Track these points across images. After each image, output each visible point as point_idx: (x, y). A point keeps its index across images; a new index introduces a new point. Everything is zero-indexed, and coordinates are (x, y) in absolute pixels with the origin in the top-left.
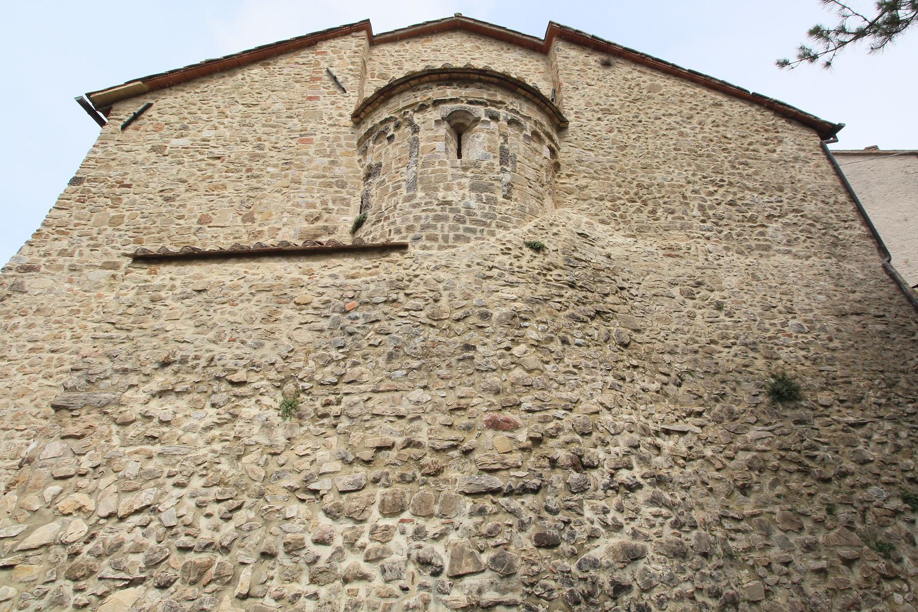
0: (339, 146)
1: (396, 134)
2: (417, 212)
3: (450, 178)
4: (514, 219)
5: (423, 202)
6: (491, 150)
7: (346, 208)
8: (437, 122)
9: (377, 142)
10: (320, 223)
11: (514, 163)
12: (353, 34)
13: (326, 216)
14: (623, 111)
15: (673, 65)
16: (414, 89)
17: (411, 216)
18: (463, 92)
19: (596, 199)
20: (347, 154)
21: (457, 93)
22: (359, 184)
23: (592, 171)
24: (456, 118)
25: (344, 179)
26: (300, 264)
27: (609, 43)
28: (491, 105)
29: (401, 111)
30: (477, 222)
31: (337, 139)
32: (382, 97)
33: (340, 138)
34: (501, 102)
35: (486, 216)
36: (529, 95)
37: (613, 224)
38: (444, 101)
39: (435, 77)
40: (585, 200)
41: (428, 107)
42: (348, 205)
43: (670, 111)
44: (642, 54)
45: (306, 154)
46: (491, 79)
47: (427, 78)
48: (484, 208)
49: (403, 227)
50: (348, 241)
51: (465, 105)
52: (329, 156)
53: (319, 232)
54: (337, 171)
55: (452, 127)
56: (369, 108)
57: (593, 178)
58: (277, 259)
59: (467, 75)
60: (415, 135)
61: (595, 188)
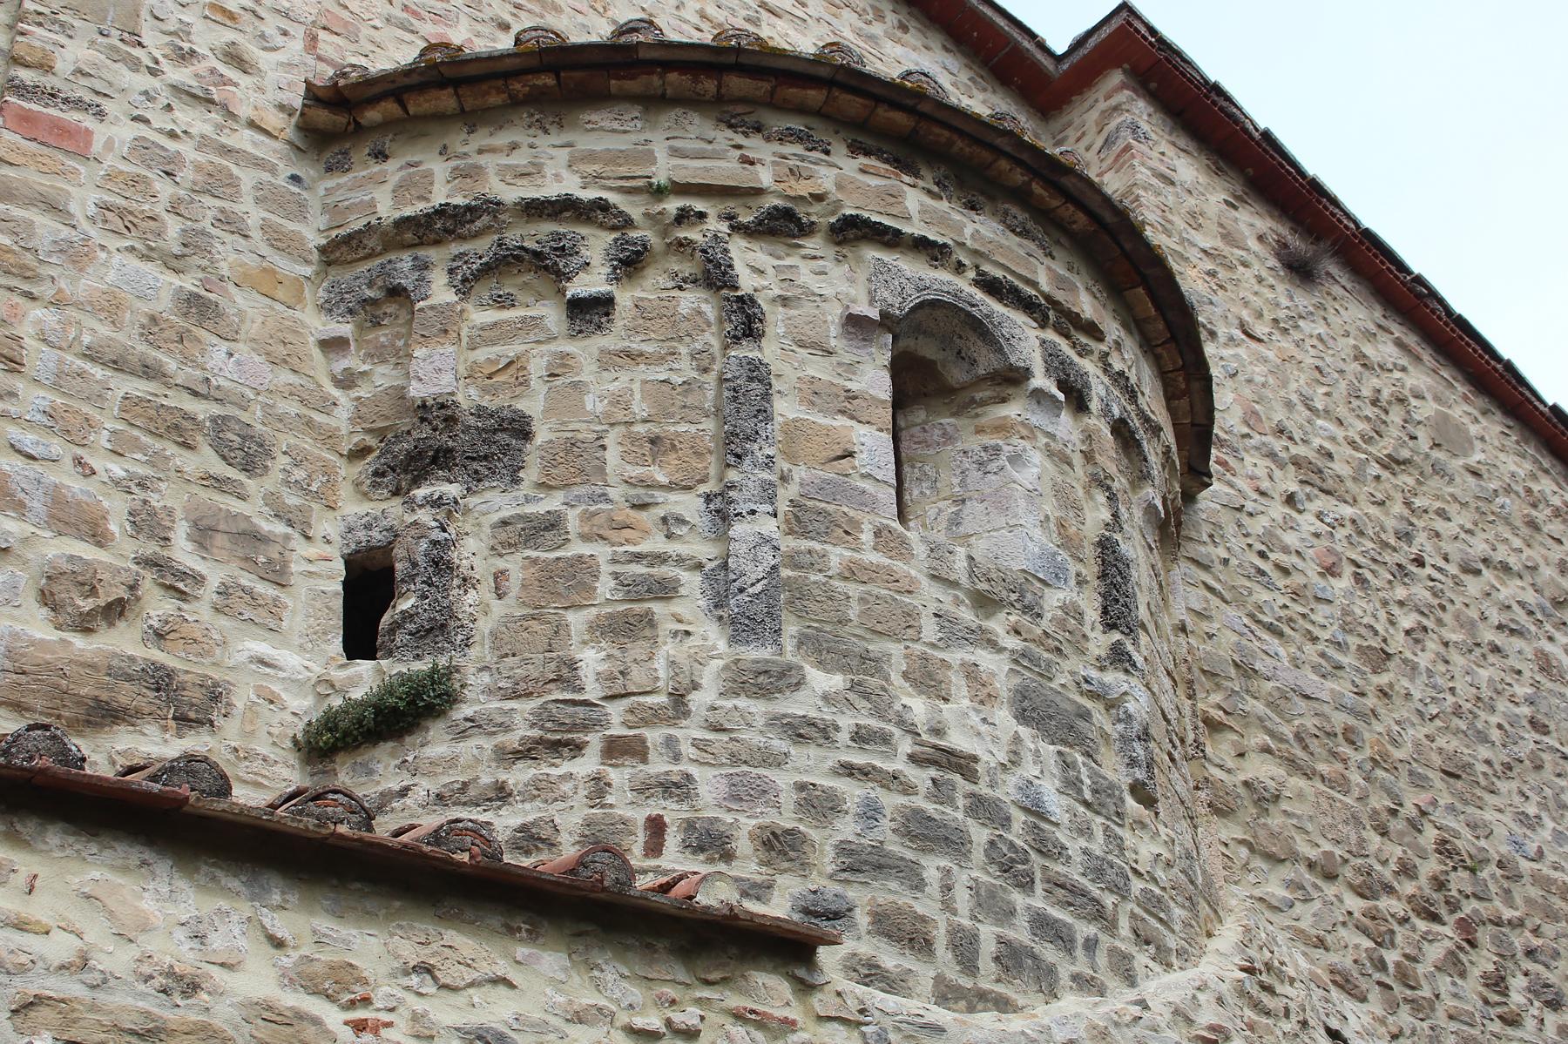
0: (227, 221)
1: (625, 298)
2: (814, 764)
3: (930, 629)
5: (847, 722)
6: (1069, 543)
7: (264, 589)
8: (855, 324)
9: (483, 291)
10: (123, 642)
13: (157, 606)
14: (1362, 492)
15: (1509, 366)
16: (735, 113)
17: (783, 780)
18: (977, 230)
19: (1311, 865)
20: (266, 283)
21: (943, 220)
22: (328, 471)
23: (1287, 731)
25: (253, 416)
26: (280, 924)
27: (1316, 187)
29: (659, 192)
31: (217, 184)
32: (548, 80)
33: (233, 183)
35: (1097, 870)
38: (889, 238)
39: (852, 105)
40: (1274, 859)
41: (806, 230)
42: (277, 575)
43: (1502, 554)
44: (1419, 280)
45: (54, 207)
47: (814, 96)
49: (744, 826)
50: (263, 779)
51: (964, 285)
52: (173, 262)
53: (126, 695)
54: (221, 362)
56: (446, 100)
58: (134, 854)
59: (986, 155)
60: (746, 351)
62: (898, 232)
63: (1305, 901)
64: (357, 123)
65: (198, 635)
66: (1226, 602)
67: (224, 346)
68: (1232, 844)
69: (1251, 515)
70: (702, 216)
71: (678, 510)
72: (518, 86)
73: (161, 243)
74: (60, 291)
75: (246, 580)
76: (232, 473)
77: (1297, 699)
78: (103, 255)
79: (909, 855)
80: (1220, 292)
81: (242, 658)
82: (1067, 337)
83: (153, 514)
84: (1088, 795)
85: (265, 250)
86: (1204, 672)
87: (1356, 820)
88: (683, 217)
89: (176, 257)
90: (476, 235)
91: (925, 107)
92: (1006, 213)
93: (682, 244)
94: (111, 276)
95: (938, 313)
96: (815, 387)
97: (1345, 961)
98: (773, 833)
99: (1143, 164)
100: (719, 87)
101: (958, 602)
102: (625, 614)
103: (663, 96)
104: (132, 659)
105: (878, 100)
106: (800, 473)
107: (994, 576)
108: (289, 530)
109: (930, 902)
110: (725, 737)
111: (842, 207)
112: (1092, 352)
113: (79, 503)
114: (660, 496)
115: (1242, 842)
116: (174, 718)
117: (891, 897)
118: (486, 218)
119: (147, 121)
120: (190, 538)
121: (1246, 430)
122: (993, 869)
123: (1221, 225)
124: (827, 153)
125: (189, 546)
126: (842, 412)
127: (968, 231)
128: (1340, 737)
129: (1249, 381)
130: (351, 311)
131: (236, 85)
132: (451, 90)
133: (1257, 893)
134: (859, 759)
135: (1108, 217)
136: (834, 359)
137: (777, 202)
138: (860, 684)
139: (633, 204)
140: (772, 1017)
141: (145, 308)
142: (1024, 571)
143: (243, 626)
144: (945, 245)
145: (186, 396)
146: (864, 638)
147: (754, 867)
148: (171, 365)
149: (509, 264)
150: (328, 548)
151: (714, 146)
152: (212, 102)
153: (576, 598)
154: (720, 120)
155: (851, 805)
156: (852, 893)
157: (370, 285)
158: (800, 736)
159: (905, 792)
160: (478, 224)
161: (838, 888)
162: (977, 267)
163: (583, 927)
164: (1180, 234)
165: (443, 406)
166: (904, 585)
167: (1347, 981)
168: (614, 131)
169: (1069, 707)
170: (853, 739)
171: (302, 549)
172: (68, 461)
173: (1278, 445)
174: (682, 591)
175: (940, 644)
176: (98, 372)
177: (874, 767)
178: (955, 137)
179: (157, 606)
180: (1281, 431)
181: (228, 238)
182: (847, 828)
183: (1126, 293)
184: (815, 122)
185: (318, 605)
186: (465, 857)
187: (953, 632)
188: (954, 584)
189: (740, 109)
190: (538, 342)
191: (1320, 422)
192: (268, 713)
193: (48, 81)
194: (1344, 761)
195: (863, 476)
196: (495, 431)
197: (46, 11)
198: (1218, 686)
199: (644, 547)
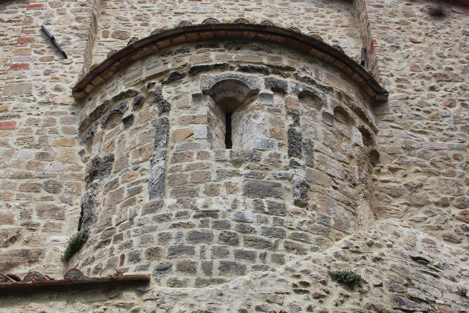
1: (136, 114)
2: (164, 227)
3: (214, 176)
5: (174, 213)
8: (196, 97)
9: (109, 125)
11: (310, 153)
16: (163, 52)
17: (155, 234)
19: (437, 204)
20: (63, 143)
21: (225, 57)
22: (78, 186)
23: (427, 163)
24: (223, 90)
28: (274, 73)
29: (143, 82)
30: (255, 242)
32: (118, 64)
35: (268, 232)
36: (328, 57)
38: (206, 69)
39: (193, 36)
40: (419, 206)
41: (183, 76)
42: (61, 217)
46: (274, 37)
47: (182, 38)
48: (266, 221)
53: (15, 260)
54: (48, 167)
55: (217, 103)
56: (99, 79)
60: (164, 116)
62: (207, 66)
63: (433, 216)
64: (87, 93)
65: (37, 239)
66: (402, 129)
67: (49, 163)
68: (400, 206)
69: (413, 99)
70: (154, 84)
71: (143, 167)
72: (112, 68)
73: (33, 143)
74: (5, 164)
75: (52, 221)
76: (50, 195)
77: (431, 151)
78: (17, 151)
79: (191, 245)
80: (403, 33)
81: (49, 241)
82: (279, 74)
83: (26, 212)
84: (266, 210)
85: (63, 135)
86: (389, 154)
87: (458, 184)
88: (149, 86)
89: (38, 145)
90: (106, 111)
91: (213, 28)
92: (252, 46)
93: (150, 93)
94: (19, 156)
95: (226, 83)
96: (183, 119)
97: (451, 232)
98: (151, 250)
99: (369, 5)
100: (157, 46)
101: (226, 166)
102: (129, 200)
103: (147, 55)
104: (17, 250)
105: (199, 31)
106: (177, 145)
107: (240, 154)
108: (66, 204)
109: (196, 257)
110: (142, 227)
111: (191, 65)
112: (290, 75)
113: (5, 215)
114: (140, 165)
115: (404, 204)
116: (28, 262)
117: (184, 259)
118: (106, 106)
119: (31, 114)
120: (37, 215)
121: (412, 72)
122: (221, 242)
123: (404, 12)
124: (189, 52)
125: (37, 217)
126: (191, 123)
127: (233, 57)
128: (452, 159)
129: (414, 57)
130: (85, 142)
131: (57, 96)
132: (99, 76)
133: (411, 218)
134: (177, 222)
135: (289, 34)
136: (190, 109)
137: (172, 72)
138: (180, 200)
139: (138, 88)
140: (127, 303)
141: (27, 161)
142: (254, 149)
143: (51, 233)
144: (224, 64)
145: (38, 179)
146: (192, 186)
147: (146, 261)
148: (33, 172)
149: (113, 116)
150: (77, 206)
151: (158, 63)
152: (51, 102)
153: (119, 200)
154: (160, 55)
155: (174, 236)
156: (172, 261)
157: (88, 134)
158: (161, 220)
159: (191, 227)
160: (105, 108)
161: (168, 261)
162: (239, 66)
163: (74, 292)
164: (385, 21)
165: (96, 160)
166: (206, 166)
167: (450, 238)
168: (135, 70)
169: (269, 185)
170: (176, 216)
171: (69, 208)
172: (4, 206)
173: (426, 73)
174: (143, 189)
175: (218, 180)
176: (14, 181)
177: (181, 223)
178: (227, 32)
179: (26, 234)
180: (428, 68)
181: (52, 135)
182: (172, 243)
183: (311, 52)
184: (183, 45)
185: (72, 222)
186: (31, 282)
187: (221, 174)
188: (225, 161)
189: (165, 50)
190: (118, 134)
191: (446, 60)
192: (55, 254)
193: (8, 113)
194: (453, 166)
195: (196, 139)
196: (107, 162)
197: (7, 96)
198: (396, 157)
199: (137, 180)
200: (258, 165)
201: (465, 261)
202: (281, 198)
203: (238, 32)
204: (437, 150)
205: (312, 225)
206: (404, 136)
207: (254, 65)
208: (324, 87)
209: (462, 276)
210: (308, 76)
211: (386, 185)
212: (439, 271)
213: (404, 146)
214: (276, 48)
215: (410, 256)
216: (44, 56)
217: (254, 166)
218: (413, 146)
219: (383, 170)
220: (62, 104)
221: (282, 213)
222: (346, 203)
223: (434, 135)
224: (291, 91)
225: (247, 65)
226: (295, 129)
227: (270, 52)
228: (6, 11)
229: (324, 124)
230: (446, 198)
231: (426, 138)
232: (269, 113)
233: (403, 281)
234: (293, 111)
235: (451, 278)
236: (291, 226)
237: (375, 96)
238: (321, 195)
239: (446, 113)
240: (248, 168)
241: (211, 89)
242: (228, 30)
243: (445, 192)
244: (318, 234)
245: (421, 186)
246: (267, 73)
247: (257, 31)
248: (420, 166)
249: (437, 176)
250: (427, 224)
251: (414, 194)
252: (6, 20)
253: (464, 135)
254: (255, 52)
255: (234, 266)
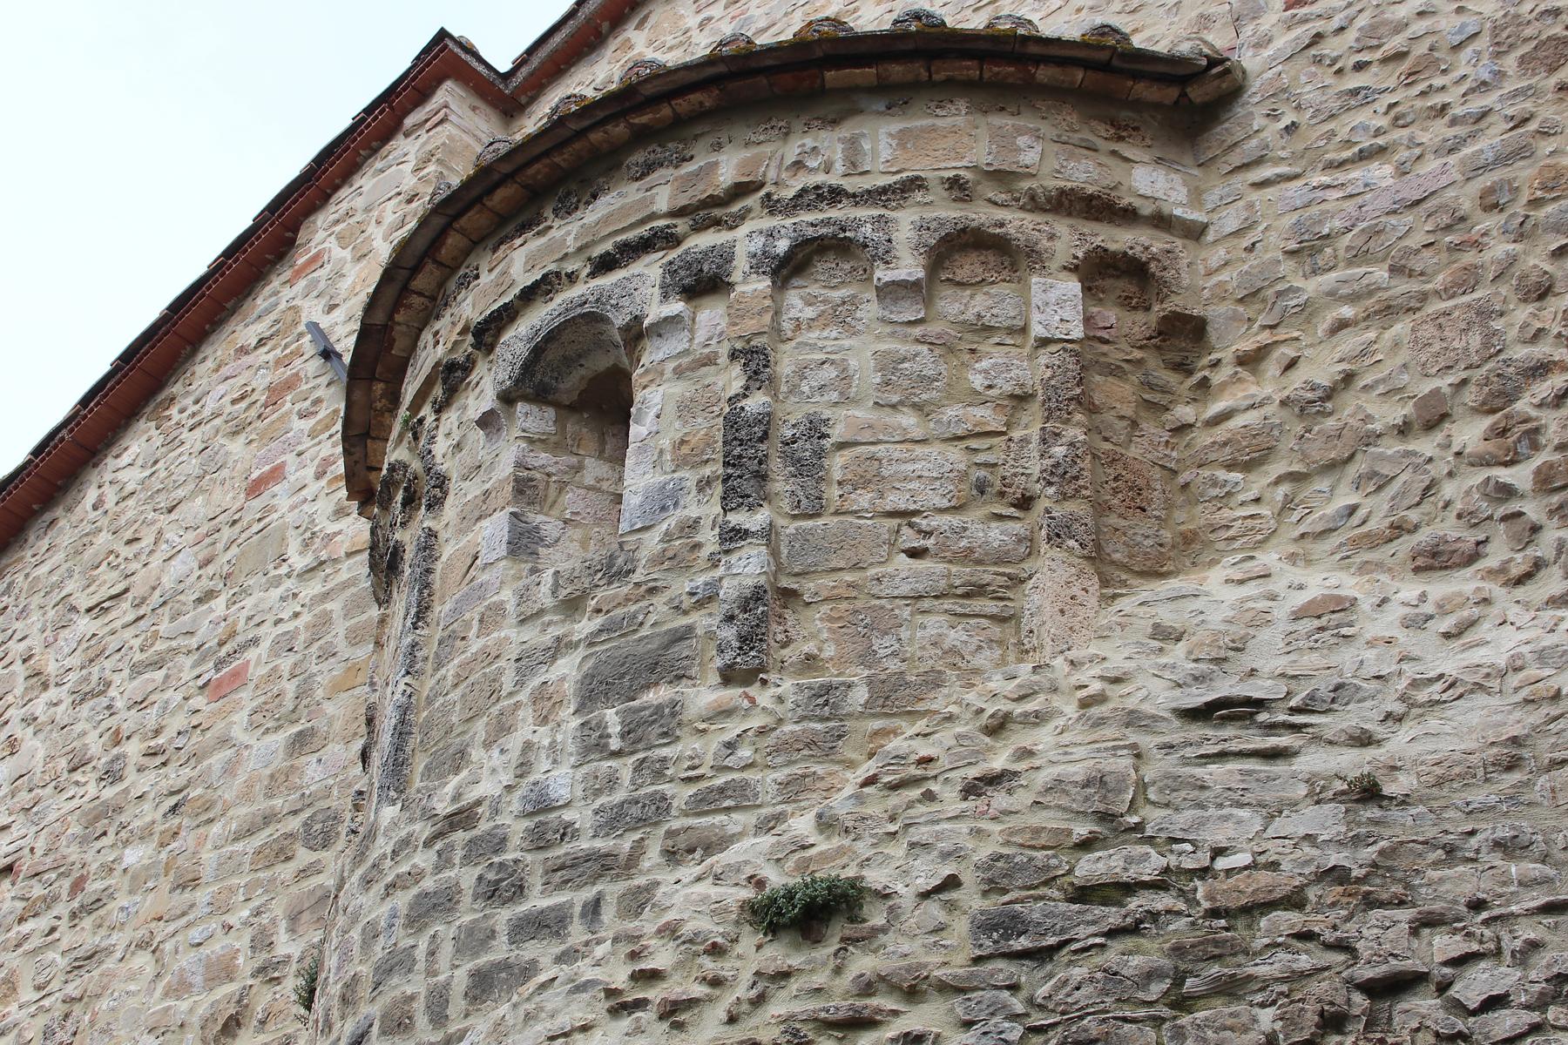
4: (767, 781)
11: (808, 468)
12: (409, 122)
19: (1404, 430)
24: (569, 362)
28: (698, 228)
30: (566, 872)
34: (741, 190)
36: (896, 71)
37: (1496, 555)
39: (474, 220)
40: (1333, 466)
46: (683, 105)
47: (453, 241)
48: (612, 782)
55: (567, 409)
57: (1388, 312)
61: (1403, 361)
63: (1380, 488)
67: (314, 758)
77: (1393, 220)
82: (717, 223)
91: (506, 168)
95: (567, 336)
100: (420, 294)
112: (749, 210)
127: (570, 240)
144: (545, 276)
145: (291, 818)
200: (625, 590)
201: (1459, 634)
202: (690, 678)
203: (577, 146)
204: (1418, 202)
205: (770, 740)
206: (1298, 203)
207: (623, 237)
208: (884, 190)
209: (1415, 711)
210: (820, 178)
211: (1221, 433)
212: (1306, 725)
213: (1293, 246)
214: (702, 135)
215: (1175, 710)
216: (320, 416)
217: (615, 596)
218: (1326, 231)
219: (1217, 378)
220: (349, 555)
221: (665, 734)
222: (959, 591)
223: (1412, 143)
224: (747, 269)
225: (608, 246)
226: (742, 409)
227: (684, 160)
228: (256, 313)
229: (888, 329)
230: (1436, 392)
231: (1380, 172)
232: (680, 383)
233: (1069, 833)
234: (748, 342)
235: (1352, 738)
236: (694, 768)
237: (1183, 95)
238: (844, 605)
239: (1463, 26)
240: (599, 611)
241: (517, 381)
242: (546, 154)
243: (1434, 370)
244: (790, 763)
245: (1348, 378)
246: (672, 240)
247: (623, 114)
248: (1353, 298)
249: (1415, 310)
250: (1357, 531)
251: (1316, 428)
252: (254, 342)
253: (1530, 87)
254: (637, 184)
255: (503, 975)
